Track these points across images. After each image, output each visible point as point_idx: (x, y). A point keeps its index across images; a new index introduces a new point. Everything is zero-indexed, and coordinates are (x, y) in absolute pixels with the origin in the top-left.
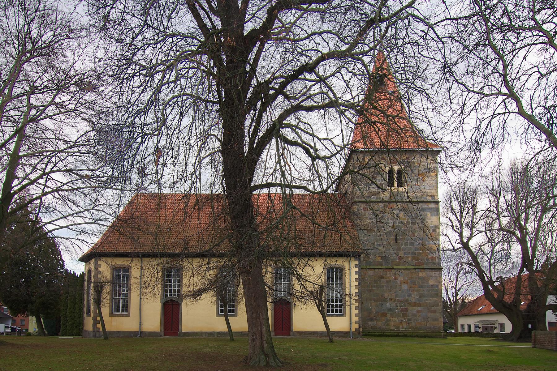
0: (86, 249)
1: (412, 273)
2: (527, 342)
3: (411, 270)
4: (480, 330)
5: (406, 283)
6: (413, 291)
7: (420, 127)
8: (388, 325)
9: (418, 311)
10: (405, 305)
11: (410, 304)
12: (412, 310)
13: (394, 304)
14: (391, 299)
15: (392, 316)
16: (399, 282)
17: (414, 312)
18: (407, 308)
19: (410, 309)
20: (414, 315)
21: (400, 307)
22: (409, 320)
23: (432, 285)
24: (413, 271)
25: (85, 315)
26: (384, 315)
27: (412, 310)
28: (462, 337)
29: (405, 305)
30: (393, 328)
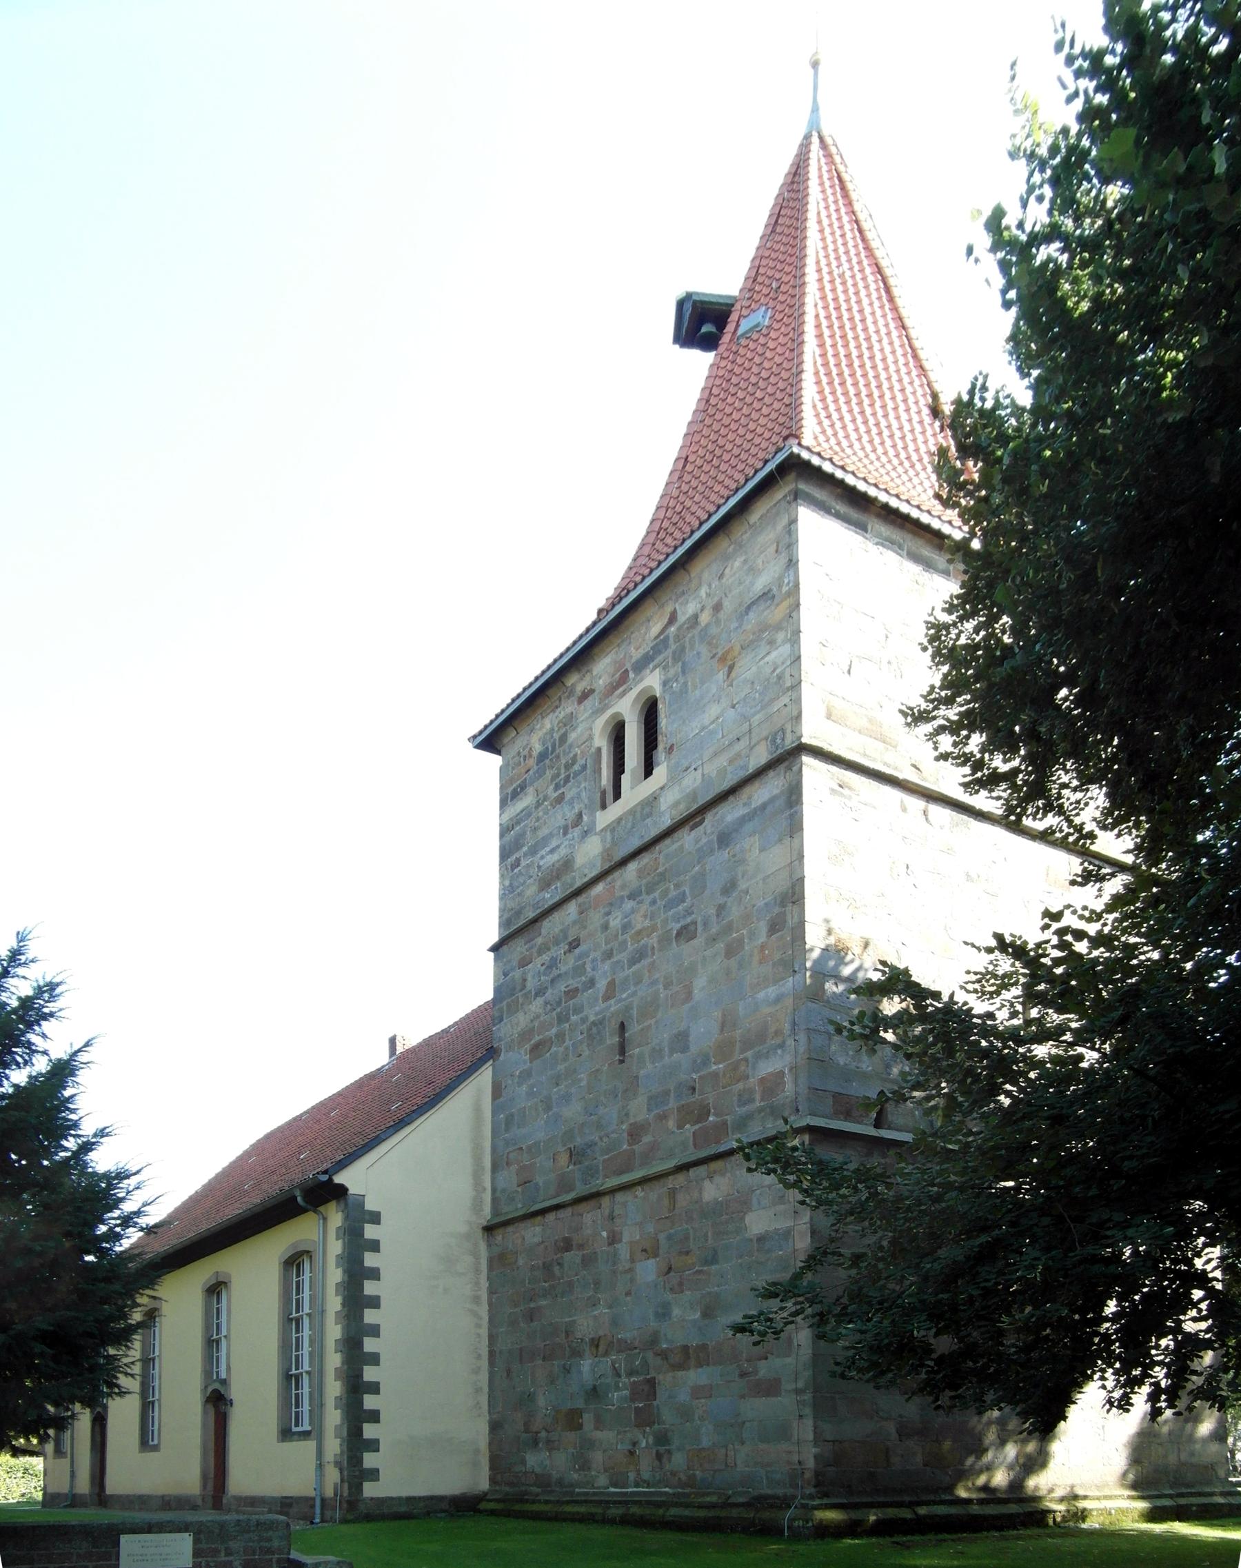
0: (660, 706)
1: (672, 1193)
2: (703, 302)
3: (671, 1182)
4: (1205, 1313)
5: (650, 1251)
6: (679, 1288)
7: (338, 1384)
8: (585, 1466)
9: (697, 1392)
10: (645, 1362)
11: (664, 1355)
12: (681, 1386)
13: (606, 1364)
14: (595, 1343)
15: (599, 1424)
16: (623, 1250)
17: (683, 1396)
18: (652, 1383)
19: (665, 1379)
20: (685, 1413)
21: (630, 1374)
22: (662, 1439)
23: (761, 1239)
24: (680, 1179)
25: (212, 1475)
26: (573, 1420)
27: (681, 1386)
28: (883, 498)
29: (645, 1362)
30: (602, 1481)
